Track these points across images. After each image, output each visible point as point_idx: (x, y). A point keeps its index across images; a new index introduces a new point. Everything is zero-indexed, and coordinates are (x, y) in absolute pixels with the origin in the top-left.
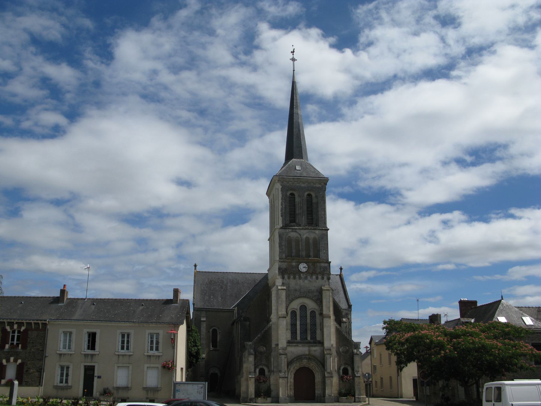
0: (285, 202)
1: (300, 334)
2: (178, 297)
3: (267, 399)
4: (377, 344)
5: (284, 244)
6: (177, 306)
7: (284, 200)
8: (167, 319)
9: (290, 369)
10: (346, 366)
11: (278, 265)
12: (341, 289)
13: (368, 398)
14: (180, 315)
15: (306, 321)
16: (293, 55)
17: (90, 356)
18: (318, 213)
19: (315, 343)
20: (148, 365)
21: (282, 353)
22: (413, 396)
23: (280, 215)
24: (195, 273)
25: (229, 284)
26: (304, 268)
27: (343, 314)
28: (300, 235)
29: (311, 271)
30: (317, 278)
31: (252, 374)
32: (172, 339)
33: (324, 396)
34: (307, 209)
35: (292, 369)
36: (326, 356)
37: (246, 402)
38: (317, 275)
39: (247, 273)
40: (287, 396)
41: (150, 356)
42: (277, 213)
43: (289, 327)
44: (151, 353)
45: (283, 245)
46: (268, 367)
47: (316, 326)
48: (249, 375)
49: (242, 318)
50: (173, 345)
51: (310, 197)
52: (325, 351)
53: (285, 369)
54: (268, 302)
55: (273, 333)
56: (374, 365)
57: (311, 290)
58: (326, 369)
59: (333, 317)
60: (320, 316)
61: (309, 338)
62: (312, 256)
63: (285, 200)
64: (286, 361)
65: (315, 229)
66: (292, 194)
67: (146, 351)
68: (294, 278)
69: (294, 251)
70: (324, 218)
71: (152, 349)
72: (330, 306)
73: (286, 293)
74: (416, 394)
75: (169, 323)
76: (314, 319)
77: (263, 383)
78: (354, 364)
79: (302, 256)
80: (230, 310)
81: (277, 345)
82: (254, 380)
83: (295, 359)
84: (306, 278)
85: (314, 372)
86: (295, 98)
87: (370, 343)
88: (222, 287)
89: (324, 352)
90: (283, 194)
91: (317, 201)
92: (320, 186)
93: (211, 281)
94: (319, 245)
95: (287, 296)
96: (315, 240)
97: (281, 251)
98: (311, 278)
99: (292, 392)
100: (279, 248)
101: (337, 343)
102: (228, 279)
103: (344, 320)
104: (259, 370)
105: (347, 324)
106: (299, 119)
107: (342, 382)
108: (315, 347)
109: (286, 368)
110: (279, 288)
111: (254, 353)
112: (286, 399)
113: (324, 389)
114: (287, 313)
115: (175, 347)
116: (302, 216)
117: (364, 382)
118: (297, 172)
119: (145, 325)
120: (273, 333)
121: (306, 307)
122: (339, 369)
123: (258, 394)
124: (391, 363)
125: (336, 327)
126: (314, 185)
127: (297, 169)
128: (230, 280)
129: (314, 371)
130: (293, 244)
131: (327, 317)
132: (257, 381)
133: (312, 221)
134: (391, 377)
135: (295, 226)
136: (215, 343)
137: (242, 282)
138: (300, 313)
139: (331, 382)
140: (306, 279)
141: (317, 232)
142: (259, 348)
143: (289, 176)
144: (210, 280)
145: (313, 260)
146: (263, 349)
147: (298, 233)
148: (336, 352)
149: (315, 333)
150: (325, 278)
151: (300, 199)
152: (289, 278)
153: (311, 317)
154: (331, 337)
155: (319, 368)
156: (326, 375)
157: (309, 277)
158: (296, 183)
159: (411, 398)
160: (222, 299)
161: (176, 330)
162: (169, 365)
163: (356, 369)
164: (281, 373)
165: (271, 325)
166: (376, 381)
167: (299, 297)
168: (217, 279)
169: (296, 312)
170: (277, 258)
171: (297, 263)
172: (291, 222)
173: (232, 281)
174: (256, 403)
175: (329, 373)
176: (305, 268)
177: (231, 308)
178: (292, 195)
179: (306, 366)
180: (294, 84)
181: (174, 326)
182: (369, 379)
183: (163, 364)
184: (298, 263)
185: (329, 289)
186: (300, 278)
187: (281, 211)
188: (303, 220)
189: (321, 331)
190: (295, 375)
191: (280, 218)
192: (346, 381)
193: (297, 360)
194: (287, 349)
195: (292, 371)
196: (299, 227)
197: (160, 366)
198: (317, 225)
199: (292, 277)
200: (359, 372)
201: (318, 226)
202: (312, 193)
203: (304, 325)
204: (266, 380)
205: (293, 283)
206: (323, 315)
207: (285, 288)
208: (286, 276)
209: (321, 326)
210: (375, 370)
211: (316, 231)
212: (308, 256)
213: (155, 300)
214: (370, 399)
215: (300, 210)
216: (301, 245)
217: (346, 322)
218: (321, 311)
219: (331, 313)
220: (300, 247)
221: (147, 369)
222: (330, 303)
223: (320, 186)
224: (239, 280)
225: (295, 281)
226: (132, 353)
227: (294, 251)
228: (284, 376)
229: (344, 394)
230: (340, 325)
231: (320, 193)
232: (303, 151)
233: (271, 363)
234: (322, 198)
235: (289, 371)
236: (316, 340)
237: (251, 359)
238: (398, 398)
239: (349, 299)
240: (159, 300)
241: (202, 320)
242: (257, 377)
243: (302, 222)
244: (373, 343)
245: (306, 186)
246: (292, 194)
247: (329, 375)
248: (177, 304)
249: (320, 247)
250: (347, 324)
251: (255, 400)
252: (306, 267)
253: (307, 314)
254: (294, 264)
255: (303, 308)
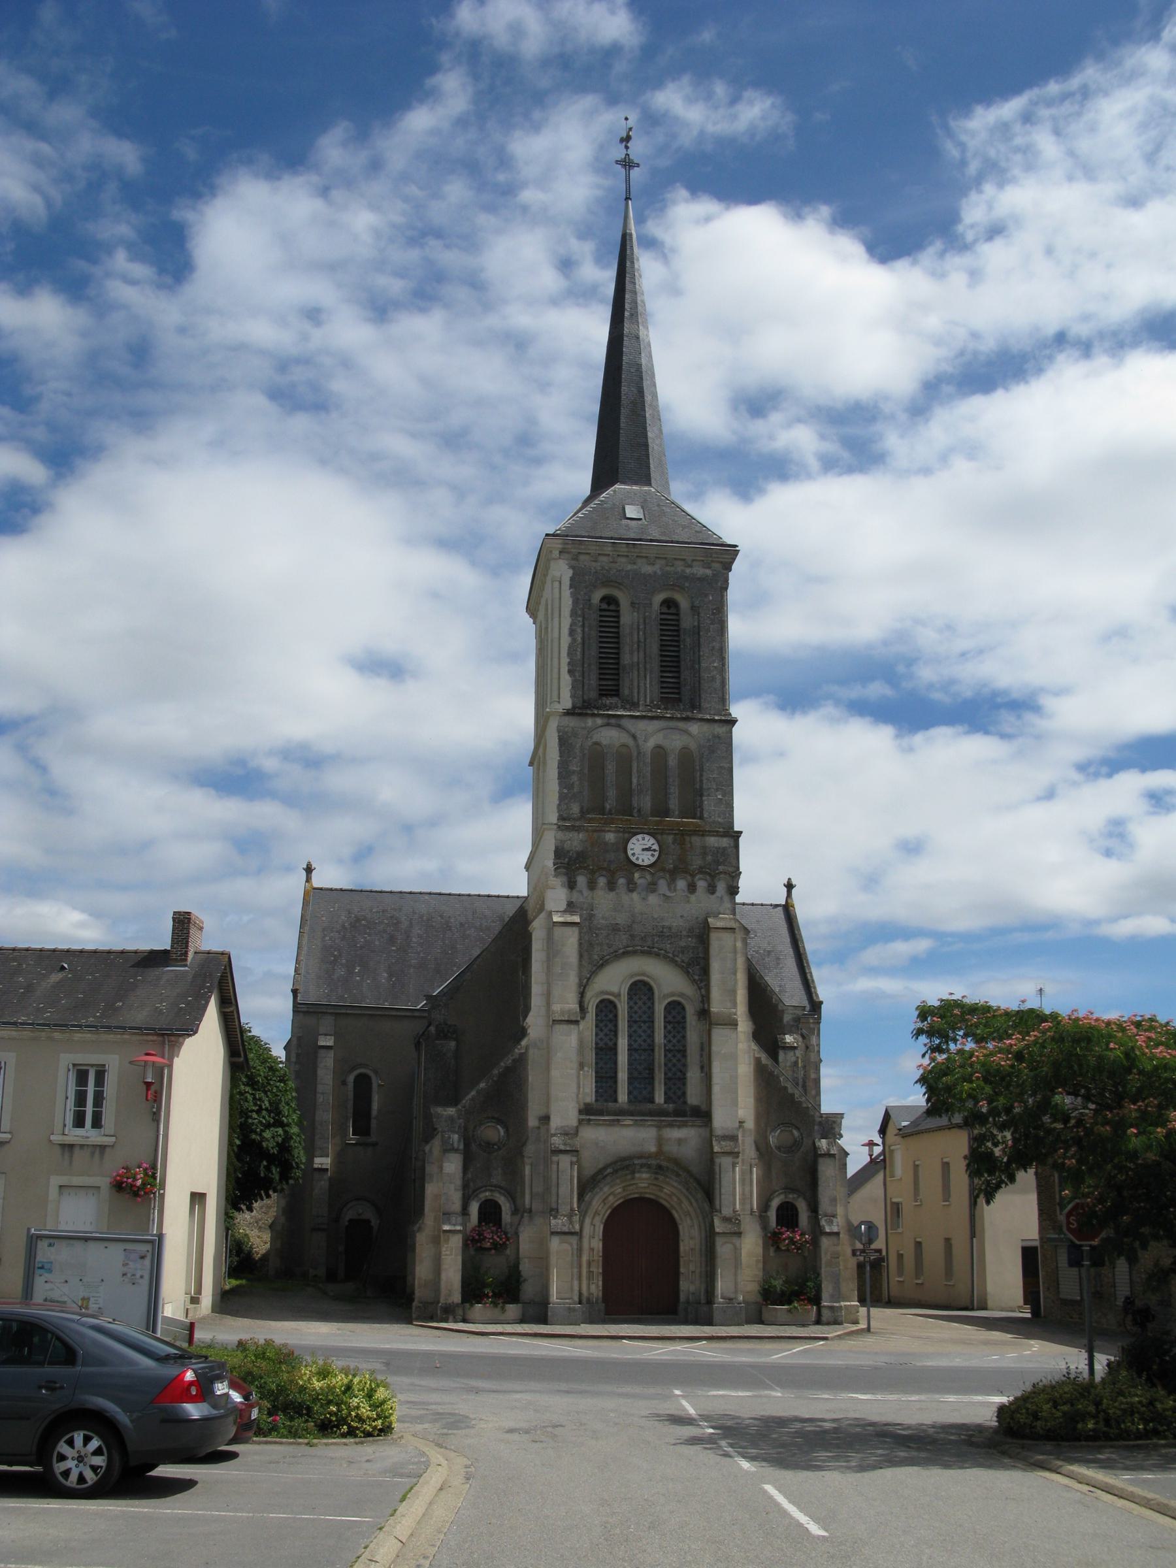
0: (583, 626)
1: (630, 1083)
2: (187, 942)
3: (503, 1310)
4: (904, 1134)
5: (579, 769)
6: (187, 971)
7: (580, 619)
8: (140, 1016)
9: (590, 1203)
10: (791, 1197)
11: (554, 841)
12: (788, 951)
13: (865, 1309)
14: (188, 1004)
15: (652, 1036)
16: (627, 148)
17: (975, 1307)
18: (699, 663)
19: (677, 1113)
20: (64, 1180)
21: (562, 1147)
22: (1021, 1302)
23: (565, 668)
24: (306, 893)
25: (417, 931)
26: (645, 852)
27: (787, 1018)
28: (634, 737)
29: (671, 861)
30: (692, 888)
31: (453, 1219)
32: (148, 1085)
33: (710, 1301)
34: (661, 651)
35: (596, 1203)
36: (717, 1161)
37: (432, 1318)
38: (693, 876)
39: (479, 896)
40: (576, 1298)
41: (71, 1147)
42: (556, 661)
43: (591, 1057)
44: (76, 1135)
45: (574, 772)
46: (512, 1196)
47: (685, 1056)
48: (444, 1223)
49: (432, 1029)
50: (155, 1110)
51: (672, 610)
52: (714, 1143)
53: (572, 1203)
54: (523, 974)
55: (533, 1077)
56: (894, 1200)
57: (670, 928)
58: (718, 1207)
59: (744, 1026)
60: (699, 1019)
61: (660, 1098)
62: (677, 813)
63: (584, 618)
64: (575, 1174)
65: (687, 719)
66: (609, 600)
67: (58, 1127)
68: (611, 886)
69: (612, 793)
70: (718, 684)
71: (79, 1122)
72: (736, 983)
73: (580, 939)
74: (1031, 1295)
75: (139, 1030)
76: (678, 1032)
77: (493, 1251)
78: (820, 1189)
79: (639, 811)
80: (417, 1014)
81: (546, 1119)
82: (461, 1241)
83: (609, 1170)
84: (652, 887)
85: (676, 1215)
86: (628, 286)
87: (883, 1131)
88: (392, 940)
89: (712, 1147)
90: (578, 599)
91: (696, 624)
92: (709, 572)
93: (358, 920)
94: (701, 775)
95: (584, 949)
96: (686, 756)
97: (565, 791)
98: (669, 886)
99: (597, 1286)
100: (560, 784)
101: (758, 1117)
102: (414, 913)
103: (789, 1039)
104: (480, 1206)
105: (798, 1053)
106: (643, 355)
107: (775, 1251)
108: (679, 1127)
109: (575, 1200)
110: (556, 919)
111: (462, 1147)
112: (574, 1310)
113: (710, 1278)
114: (583, 1009)
115: (163, 1114)
116: (642, 673)
117: (854, 1253)
118: (627, 526)
119: (57, 1035)
120: (530, 1079)
121: (650, 989)
122: (764, 1207)
123: (473, 1291)
124: (949, 1196)
125: (758, 1061)
126: (688, 571)
127: (628, 516)
128: (421, 917)
129: (677, 1211)
130: (611, 768)
131: (725, 1025)
132: (473, 1243)
133: (678, 693)
134: (948, 1241)
135: (616, 707)
136: (362, 1120)
137: (462, 925)
138: (630, 1008)
139: (737, 1251)
140: (654, 891)
141: (694, 728)
142: (483, 1127)
143: (601, 538)
144: (356, 917)
145: (678, 823)
146: (494, 1133)
147: (628, 732)
148: (753, 1147)
149: (683, 1080)
150: (721, 887)
151: (635, 614)
152: (592, 886)
153: (669, 1022)
154: (736, 1092)
155: (695, 1204)
156: (719, 1227)
157: (663, 885)
158: (623, 560)
159: (1014, 1311)
160: (391, 975)
161: (166, 1056)
162: (135, 1179)
163: (824, 1205)
164: (555, 1218)
165: (527, 1048)
166: (901, 1252)
167: (626, 954)
168: (377, 912)
169: (615, 1007)
170: (553, 817)
171: (621, 834)
172: (604, 693)
173: (428, 920)
174: (464, 1321)
175: (726, 1220)
176: (650, 853)
177: (418, 1007)
178: (609, 604)
179: (647, 1196)
180: (628, 242)
181: (160, 1038)
182: (870, 1241)
183: (115, 1174)
184: (626, 835)
185: (733, 924)
186: (631, 887)
187: (569, 654)
188: (646, 687)
189: (702, 1072)
190: (607, 1225)
191: (566, 679)
192: (788, 1250)
193: (616, 1171)
194: (580, 1134)
195: (596, 1213)
196: (630, 710)
197: (104, 1182)
198: (695, 705)
199: (602, 881)
200: (835, 1220)
201: (699, 708)
202: (679, 597)
203: (645, 1050)
204: (504, 1243)
205: (604, 902)
206: (710, 1017)
207: (577, 919)
208: (581, 880)
209: (701, 1056)
210: (898, 1216)
211: (689, 724)
212: (662, 810)
213: (109, 952)
214: (874, 1311)
215: (636, 653)
216: (637, 771)
217: (795, 1048)
218: (703, 1002)
219: (741, 1010)
220: (635, 781)
221: (60, 1193)
222: (735, 973)
223: (709, 572)
224: (449, 917)
225: (612, 895)
226: (9, 1136)
227: (612, 793)
228: (565, 1229)
229: (783, 1293)
230: (774, 1056)
231: (706, 595)
232: (651, 461)
233: (523, 1182)
234: (713, 614)
235: (586, 1212)
236: (685, 1103)
237: (453, 1166)
238: (972, 1309)
239: (813, 981)
240: (122, 952)
241: (321, 1043)
242: (474, 1230)
243: (642, 694)
244: (891, 1130)
245: (659, 572)
246: (610, 600)
247: (728, 1228)
248: (186, 966)
249: (705, 781)
250: (799, 1056)
251: (464, 1310)
252: (655, 850)
253: (653, 1013)
254: (610, 837)
255: (641, 990)
